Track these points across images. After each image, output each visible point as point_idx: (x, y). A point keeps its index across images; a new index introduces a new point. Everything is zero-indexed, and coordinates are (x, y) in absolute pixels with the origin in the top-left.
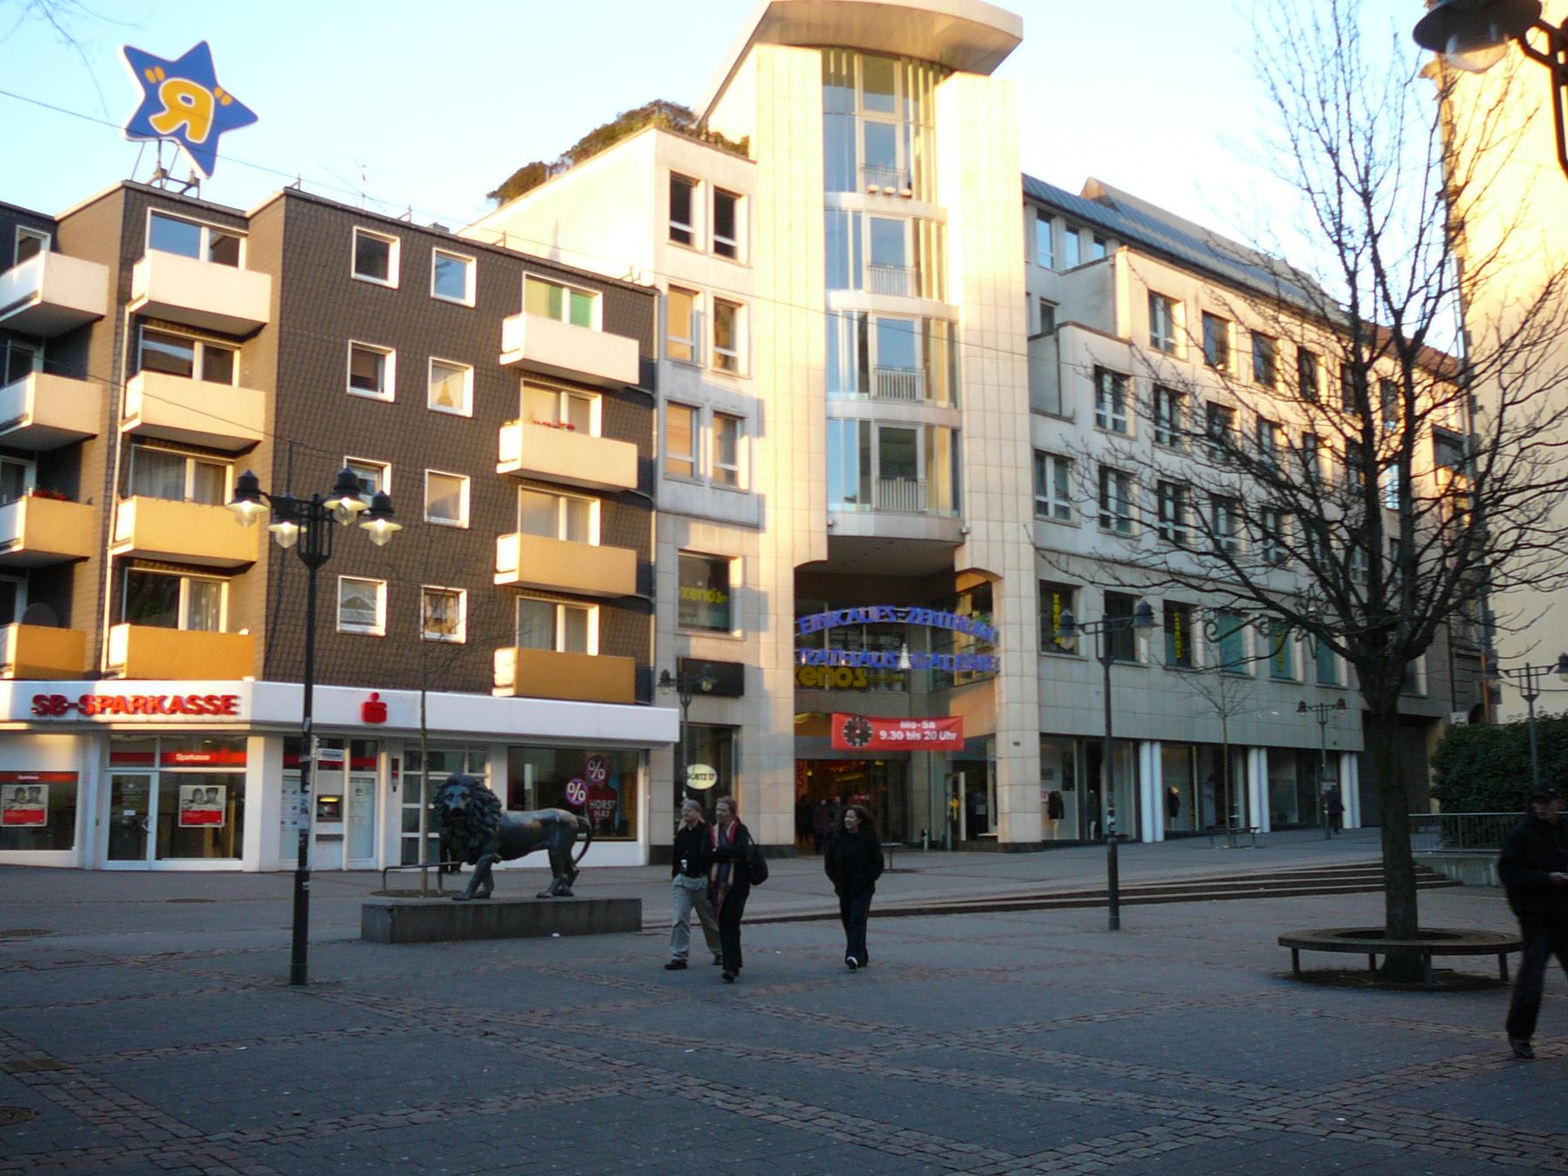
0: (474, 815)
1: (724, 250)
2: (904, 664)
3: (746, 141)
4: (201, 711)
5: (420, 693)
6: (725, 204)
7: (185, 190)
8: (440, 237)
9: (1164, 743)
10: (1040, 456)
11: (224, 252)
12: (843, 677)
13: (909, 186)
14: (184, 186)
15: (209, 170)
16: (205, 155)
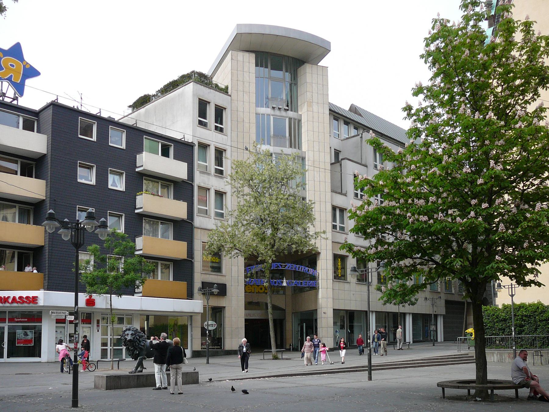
0: (137, 341)
1: (221, 130)
2: (285, 284)
3: (227, 88)
4: (23, 302)
5: (110, 295)
6: (219, 112)
7: (12, 101)
9: (376, 312)
10: (334, 208)
11: (28, 126)
13: (288, 106)
14: (12, 100)
15: (21, 94)
16: (20, 88)
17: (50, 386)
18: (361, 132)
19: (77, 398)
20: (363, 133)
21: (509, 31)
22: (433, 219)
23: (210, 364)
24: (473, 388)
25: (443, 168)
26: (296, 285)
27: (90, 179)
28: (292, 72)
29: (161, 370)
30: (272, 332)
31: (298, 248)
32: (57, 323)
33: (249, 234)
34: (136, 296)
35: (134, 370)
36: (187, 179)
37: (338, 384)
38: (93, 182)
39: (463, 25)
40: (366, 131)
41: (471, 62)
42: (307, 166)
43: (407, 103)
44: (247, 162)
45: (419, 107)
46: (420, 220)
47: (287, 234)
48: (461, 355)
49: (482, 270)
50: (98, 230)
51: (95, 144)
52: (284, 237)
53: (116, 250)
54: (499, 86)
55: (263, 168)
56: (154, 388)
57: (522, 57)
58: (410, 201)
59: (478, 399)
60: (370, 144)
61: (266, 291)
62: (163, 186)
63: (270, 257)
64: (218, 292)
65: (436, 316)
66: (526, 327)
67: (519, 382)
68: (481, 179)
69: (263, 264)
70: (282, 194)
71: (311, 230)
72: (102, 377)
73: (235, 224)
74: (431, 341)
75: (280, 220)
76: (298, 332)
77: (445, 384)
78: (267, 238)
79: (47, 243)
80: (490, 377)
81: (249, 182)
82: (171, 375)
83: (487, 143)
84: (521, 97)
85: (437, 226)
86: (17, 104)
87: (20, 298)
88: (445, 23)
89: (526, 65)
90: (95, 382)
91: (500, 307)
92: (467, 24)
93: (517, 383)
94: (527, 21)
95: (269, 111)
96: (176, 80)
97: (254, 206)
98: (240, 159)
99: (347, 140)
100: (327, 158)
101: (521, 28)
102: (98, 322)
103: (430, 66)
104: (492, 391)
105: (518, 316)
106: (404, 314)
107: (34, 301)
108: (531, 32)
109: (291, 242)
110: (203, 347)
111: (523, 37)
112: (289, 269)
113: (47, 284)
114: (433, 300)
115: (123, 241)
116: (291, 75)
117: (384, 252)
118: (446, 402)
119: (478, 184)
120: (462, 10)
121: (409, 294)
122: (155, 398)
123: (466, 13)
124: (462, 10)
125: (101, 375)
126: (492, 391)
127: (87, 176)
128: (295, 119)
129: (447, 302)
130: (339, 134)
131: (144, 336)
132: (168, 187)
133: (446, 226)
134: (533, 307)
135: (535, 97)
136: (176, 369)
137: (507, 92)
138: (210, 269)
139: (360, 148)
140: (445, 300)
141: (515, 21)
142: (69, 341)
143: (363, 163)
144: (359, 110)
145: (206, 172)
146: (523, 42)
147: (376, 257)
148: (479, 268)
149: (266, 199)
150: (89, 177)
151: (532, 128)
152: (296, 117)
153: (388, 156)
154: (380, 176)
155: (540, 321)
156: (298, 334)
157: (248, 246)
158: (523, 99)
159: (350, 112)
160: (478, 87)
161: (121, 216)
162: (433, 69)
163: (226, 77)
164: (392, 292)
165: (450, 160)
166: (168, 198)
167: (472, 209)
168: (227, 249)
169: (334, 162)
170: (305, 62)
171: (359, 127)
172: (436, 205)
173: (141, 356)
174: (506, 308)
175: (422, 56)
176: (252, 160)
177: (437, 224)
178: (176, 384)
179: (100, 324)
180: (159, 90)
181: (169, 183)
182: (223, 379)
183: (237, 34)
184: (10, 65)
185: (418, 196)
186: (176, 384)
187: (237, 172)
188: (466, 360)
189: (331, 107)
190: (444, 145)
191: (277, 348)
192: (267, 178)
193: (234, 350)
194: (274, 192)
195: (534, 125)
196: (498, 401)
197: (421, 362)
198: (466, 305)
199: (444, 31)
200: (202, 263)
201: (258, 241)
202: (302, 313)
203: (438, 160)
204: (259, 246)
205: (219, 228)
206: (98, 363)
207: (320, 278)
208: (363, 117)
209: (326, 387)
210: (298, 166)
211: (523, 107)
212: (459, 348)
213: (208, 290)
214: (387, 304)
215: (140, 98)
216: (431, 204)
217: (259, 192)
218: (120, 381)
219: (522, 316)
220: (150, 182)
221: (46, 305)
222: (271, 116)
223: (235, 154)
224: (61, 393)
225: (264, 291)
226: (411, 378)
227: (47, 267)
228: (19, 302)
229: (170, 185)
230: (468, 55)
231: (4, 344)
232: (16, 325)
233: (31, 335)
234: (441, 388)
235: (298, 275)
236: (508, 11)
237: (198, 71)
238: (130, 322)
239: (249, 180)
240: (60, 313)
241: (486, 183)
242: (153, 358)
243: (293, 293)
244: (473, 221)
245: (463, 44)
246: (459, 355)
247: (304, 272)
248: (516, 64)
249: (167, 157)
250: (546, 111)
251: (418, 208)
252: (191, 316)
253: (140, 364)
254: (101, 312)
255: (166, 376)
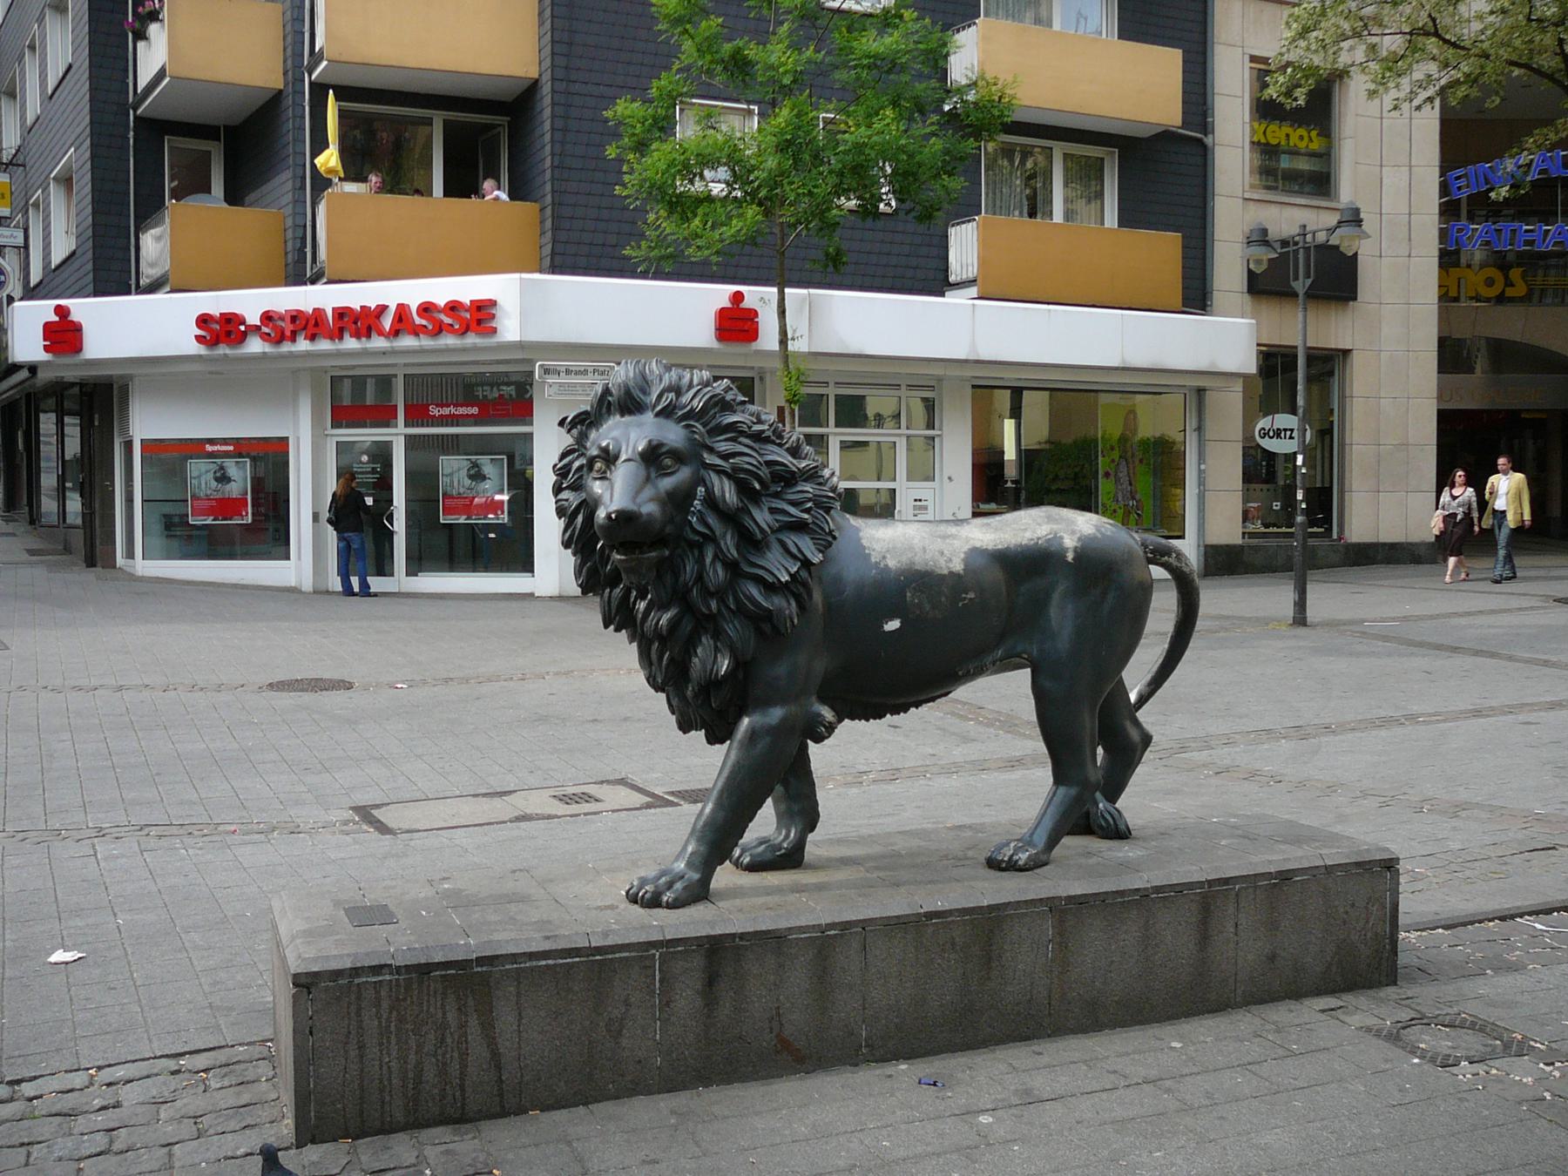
0: (711, 538)
4: (439, 329)
23: (1314, 626)
110: (1251, 528)
113: (548, 250)
193: (1385, 544)
218: (488, 1026)
225: (1504, 290)
231: (392, 514)
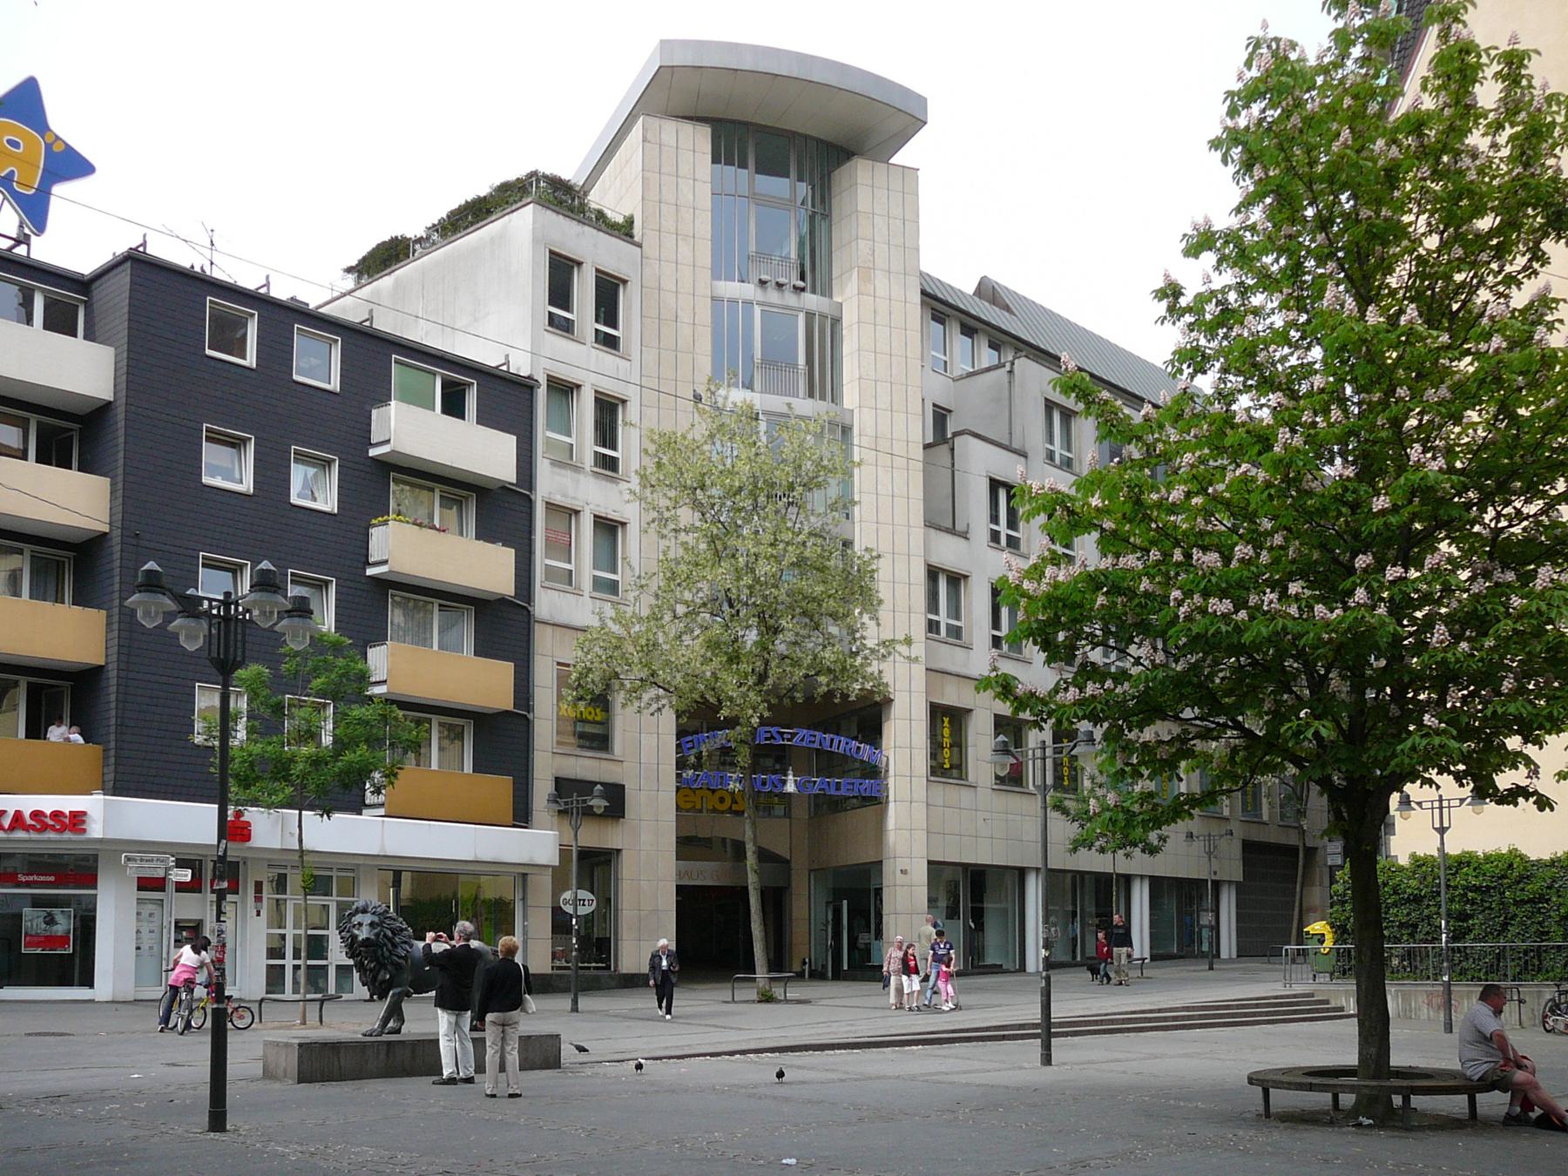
0: (385, 945)
1: (610, 342)
2: (790, 787)
3: (630, 222)
4: (45, 827)
5: (297, 812)
6: (608, 291)
8: (296, 312)
10: (933, 573)
11: (60, 321)
12: (722, 800)
13: (802, 278)
14: (12, 242)
15: (40, 228)
16: (35, 211)
17: (132, 1070)
18: (1010, 358)
19: (225, 1107)
20: (1016, 361)
21: (1465, 77)
22: (1247, 608)
23: (583, 1012)
24: (1351, 1089)
25: (1278, 464)
26: (823, 789)
27: (237, 476)
28: (817, 181)
29: (457, 1027)
30: (758, 923)
31: (832, 686)
32: (139, 889)
33: (694, 646)
34: (367, 816)
35: (376, 1026)
36: (515, 482)
37: (958, 1073)
38: (247, 485)
39: (1333, 57)
40: (1024, 354)
41: (1357, 162)
42: (856, 449)
43: (1167, 276)
44: (690, 437)
45: (1202, 289)
46: (1210, 610)
47: (803, 644)
48: (1295, 996)
49: (1385, 757)
50: (284, 622)
51: (253, 375)
52: (795, 651)
53: (317, 683)
54: (1431, 232)
55: (735, 454)
56: (435, 1078)
57: (1499, 150)
58: (1178, 555)
59: (1367, 1122)
60: (1061, 392)
61: (735, 807)
62: (446, 502)
63: (754, 709)
64: (605, 807)
65: (1217, 885)
66: (1476, 921)
67: (1480, 1074)
68: (1382, 498)
69: (733, 728)
70: (788, 529)
71: (872, 635)
72: (287, 1045)
73: (654, 613)
74: (1203, 955)
75: (783, 603)
76: (826, 926)
77: (1268, 1077)
78: (744, 655)
79: (114, 658)
80: (1397, 1059)
81: (694, 494)
82: (488, 1044)
83: (1403, 395)
84: (1494, 266)
85: (1259, 629)
86: (28, 257)
87: (35, 815)
88: (1285, 51)
89: (1514, 174)
90: (265, 1058)
91: (1404, 861)
92: (1344, 55)
93: (1476, 1077)
94: (1513, 50)
95: (749, 291)
96: (485, 197)
97: (710, 563)
98: (667, 427)
99: (973, 378)
100: (918, 430)
101: (1496, 67)
102: (259, 887)
103: (1237, 172)
104: (1406, 1100)
105: (1456, 888)
106: (1127, 879)
107: (74, 825)
108: (1524, 82)
109: (814, 669)
110: (558, 964)
111: (1502, 95)
112: (804, 744)
113: (112, 776)
114: (1210, 840)
115: (335, 657)
116: (813, 189)
117: (1104, 701)
118: (1276, 1127)
119: (1374, 510)
120: (1329, 12)
121: (1167, 820)
122: (445, 1108)
123: (1340, 24)
124: (1329, 12)
125: (285, 1040)
126: (1406, 1100)
127: (230, 466)
128: (823, 316)
129: (1249, 847)
130: (946, 362)
131: (406, 929)
132: (460, 503)
133: (1284, 628)
134: (1495, 863)
135: (1536, 265)
136: (503, 1025)
137: (1458, 252)
138: (572, 740)
139: (1007, 402)
140: (1243, 840)
141: (1483, 47)
142: (176, 941)
143: (1015, 445)
144: (1003, 295)
145: (569, 462)
146: (1502, 110)
147: (1080, 714)
148: (1373, 750)
149: (745, 546)
150: (234, 468)
151: (1531, 354)
152: (826, 310)
153: (1114, 427)
154: (1092, 483)
155: (1516, 903)
156: (826, 931)
157: (690, 678)
158: (1499, 272)
159: (977, 299)
160: (1375, 234)
161: (327, 583)
162: (1244, 180)
163: (627, 191)
164: (1121, 816)
165: (1298, 441)
166: (462, 534)
167: (1358, 581)
168: (628, 686)
169: (931, 441)
170: (854, 154)
171: (1003, 342)
172: (1253, 568)
173: (396, 987)
174: (1419, 866)
175: (1215, 144)
176: (704, 432)
177: (1257, 624)
178: (502, 1068)
179: (265, 895)
180: (434, 225)
181: (464, 493)
182: (626, 1057)
183: (660, 67)
184: (8, 141)
185: (1200, 543)
186: (502, 1068)
187: (659, 465)
188: (1309, 1011)
189: (924, 283)
190: (1274, 398)
191: (770, 971)
192: (747, 484)
194: (767, 524)
195: (1537, 343)
196: (1421, 1128)
197: (1184, 1016)
198: (1301, 855)
199: (1282, 75)
200: (555, 725)
201: (721, 662)
202: (839, 872)
203: (1259, 441)
204: (723, 675)
205: (610, 623)
206: (263, 1005)
207: (891, 772)
208: (1015, 315)
209: (927, 1081)
210: (835, 449)
211: (1500, 295)
212: (1287, 977)
213: (578, 801)
214: (1082, 849)
215: (379, 245)
216: (1237, 565)
217: (722, 523)
219: (1467, 888)
220: (408, 488)
221: (110, 836)
222: (756, 307)
223: (651, 413)
224: (171, 1089)
225: (731, 807)
226: (1158, 1060)
227: (112, 729)
228: (33, 827)
229: (466, 498)
230: (1350, 142)
232: (14, 894)
233: (64, 924)
234: (1260, 1089)
235: (829, 763)
236: (1457, 20)
237: (548, 172)
238: (350, 887)
239: (696, 489)
240: (152, 860)
241: (1395, 509)
242: (433, 993)
243: (812, 815)
244: (1363, 617)
245: (1332, 111)
246: (1287, 997)
247: (844, 755)
248: (1481, 172)
249: (458, 417)
250: (1557, 310)
251: (1204, 576)
252: (523, 875)
253: (395, 1012)
254: (269, 860)
255: (470, 1046)
